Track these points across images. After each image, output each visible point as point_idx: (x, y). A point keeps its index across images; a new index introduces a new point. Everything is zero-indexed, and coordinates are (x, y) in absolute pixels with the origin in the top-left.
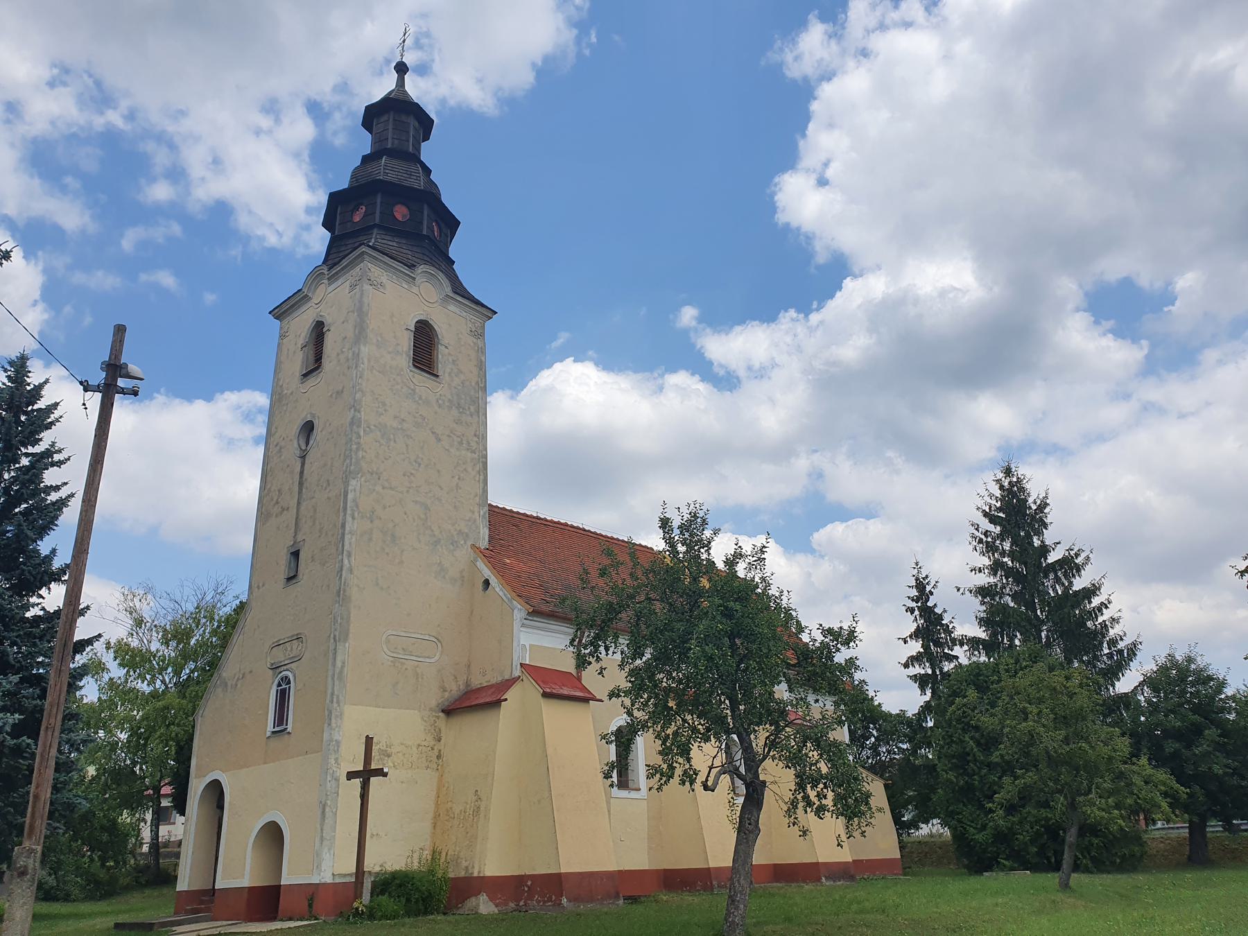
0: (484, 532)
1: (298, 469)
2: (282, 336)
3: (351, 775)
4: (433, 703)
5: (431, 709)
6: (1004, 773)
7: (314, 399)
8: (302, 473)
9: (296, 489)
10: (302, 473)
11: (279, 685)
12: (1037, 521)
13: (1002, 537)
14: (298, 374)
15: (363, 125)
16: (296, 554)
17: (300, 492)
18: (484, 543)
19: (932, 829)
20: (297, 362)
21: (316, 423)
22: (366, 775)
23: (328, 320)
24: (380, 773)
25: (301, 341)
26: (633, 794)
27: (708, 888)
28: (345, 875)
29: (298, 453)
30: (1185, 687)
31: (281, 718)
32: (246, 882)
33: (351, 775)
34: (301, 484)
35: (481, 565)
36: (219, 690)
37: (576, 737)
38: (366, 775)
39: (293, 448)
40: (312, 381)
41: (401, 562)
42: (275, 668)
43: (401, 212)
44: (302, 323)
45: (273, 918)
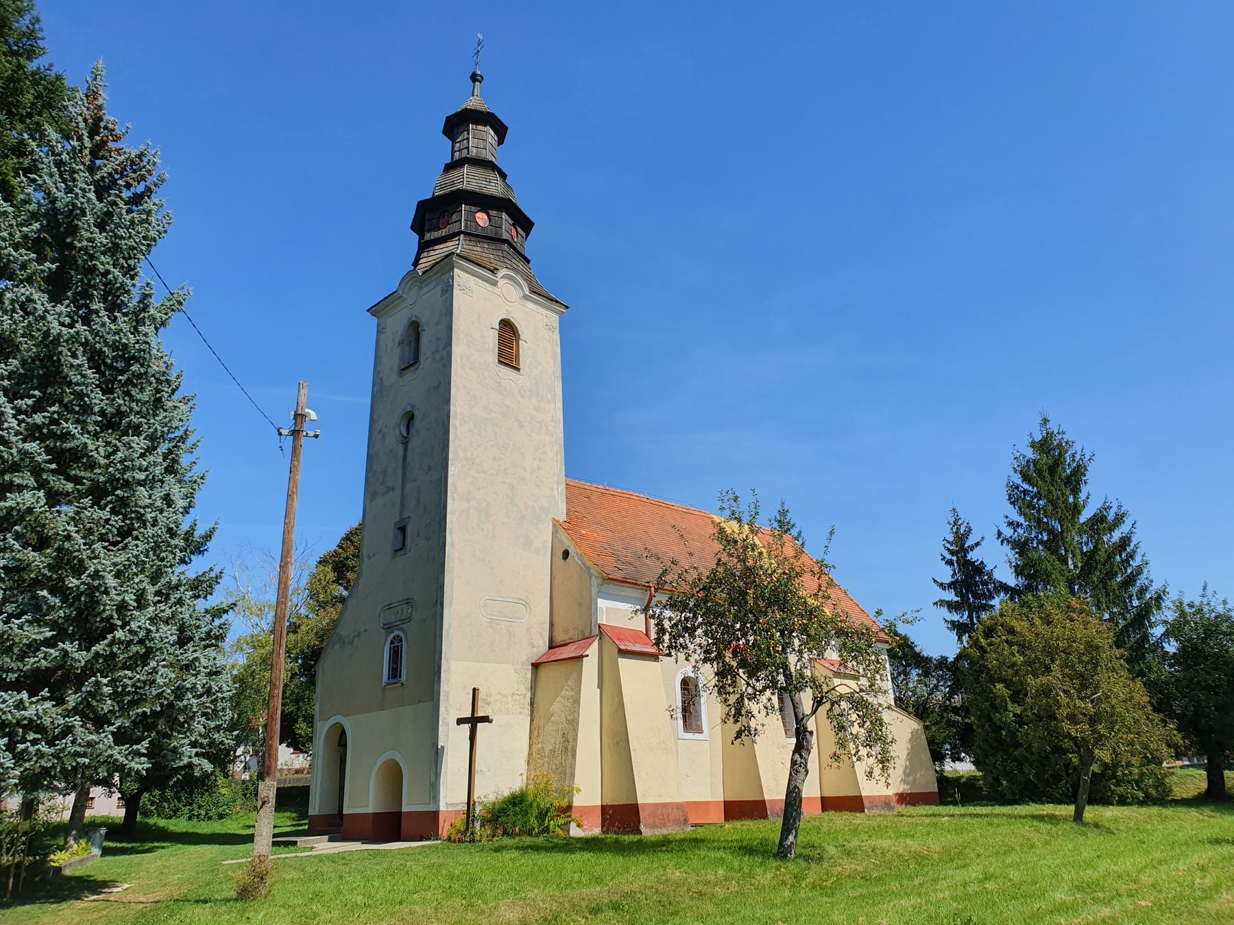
0: (563, 507)
1: (401, 454)
2: (379, 332)
3: (460, 721)
4: (524, 658)
5: (523, 663)
6: (79, 613)
7: (411, 390)
8: (405, 457)
9: (400, 471)
10: (405, 457)
11: (392, 643)
12: (1075, 479)
13: (1038, 496)
14: (396, 369)
15: (448, 119)
16: (403, 530)
17: (404, 475)
18: (562, 517)
19: (964, 768)
20: (393, 360)
21: (416, 413)
22: (473, 721)
23: (423, 320)
24: (486, 719)
25: (397, 339)
26: (697, 736)
27: (764, 815)
28: (457, 805)
29: (400, 439)
30: (1204, 639)
31: (395, 673)
32: (370, 809)
33: (460, 721)
34: (404, 467)
35: (563, 535)
36: (337, 647)
37: (650, 686)
38: (473, 721)
39: (392, 440)
40: (409, 376)
41: (494, 536)
42: (388, 628)
43: (482, 218)
44: (398, 321)
45: (398, 839)
